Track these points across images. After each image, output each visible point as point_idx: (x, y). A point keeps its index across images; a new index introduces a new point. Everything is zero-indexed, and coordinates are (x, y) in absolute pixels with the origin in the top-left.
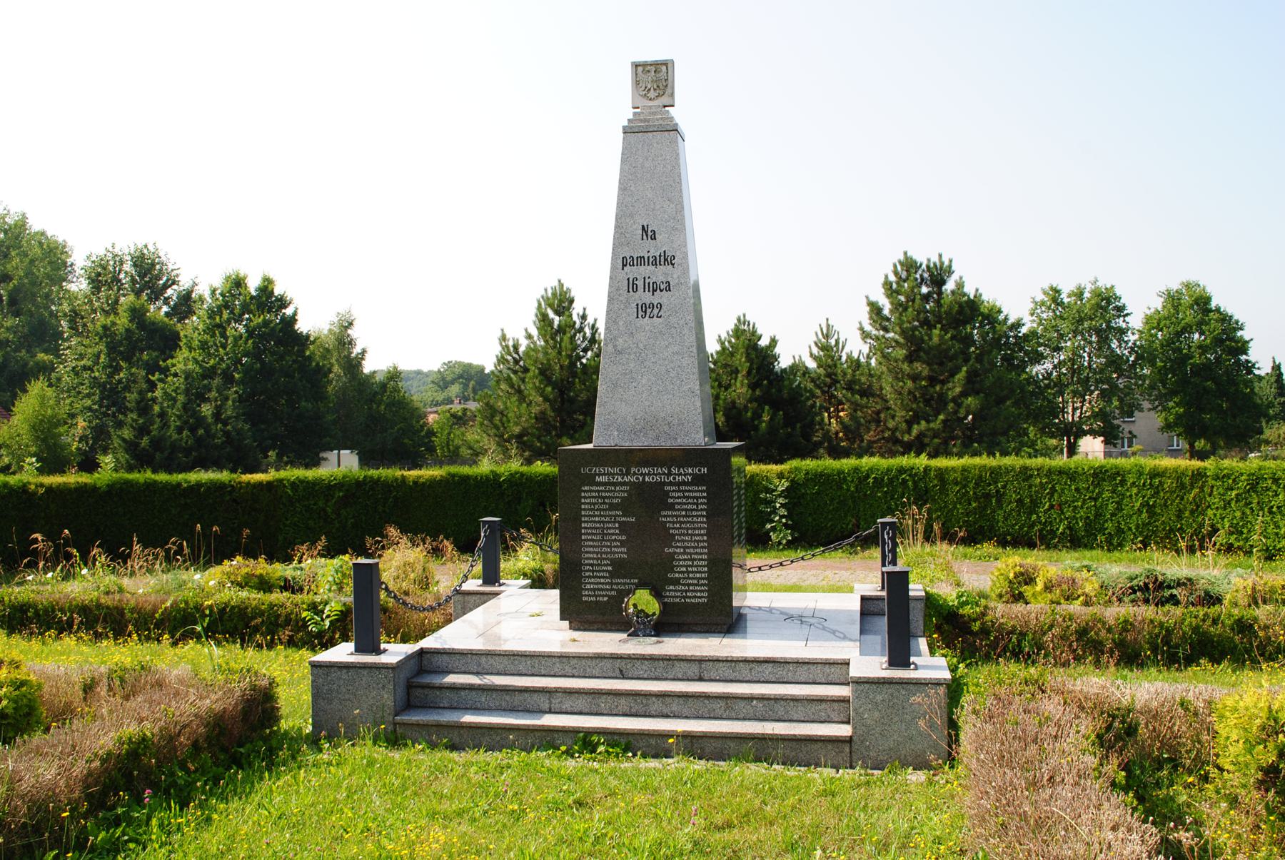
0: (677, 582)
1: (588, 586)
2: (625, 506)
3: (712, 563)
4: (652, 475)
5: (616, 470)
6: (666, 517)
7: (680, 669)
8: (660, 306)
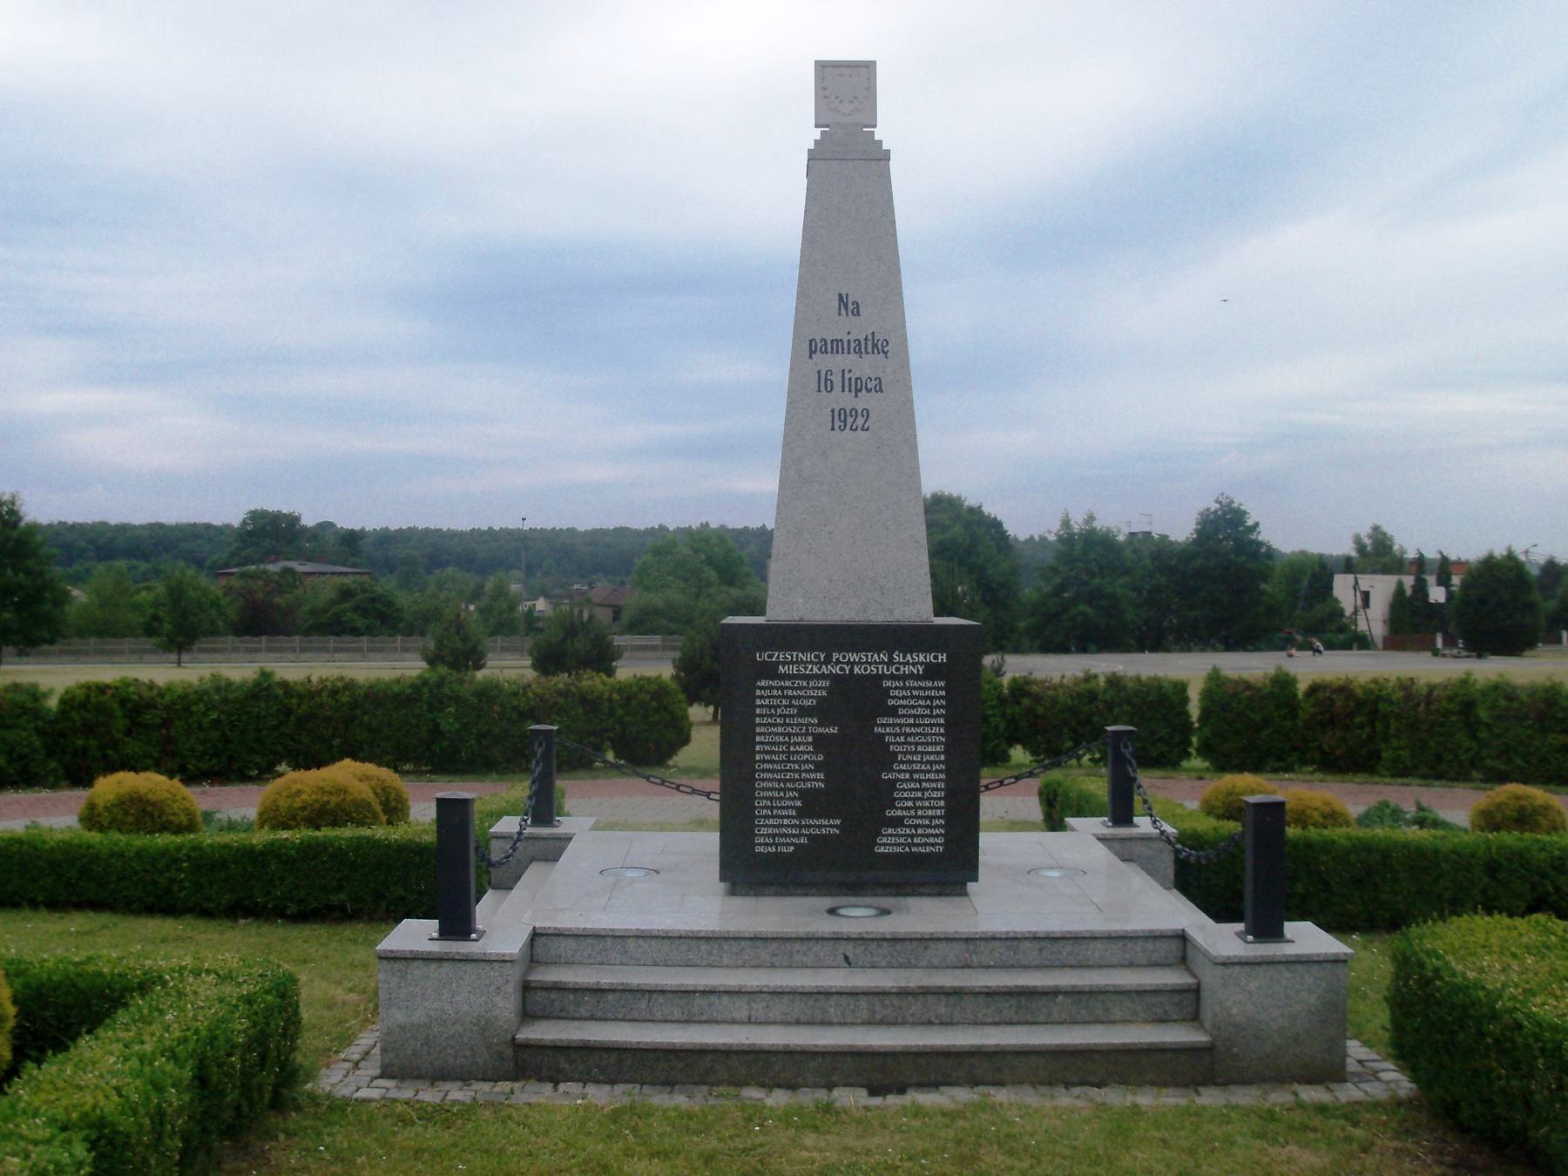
0: (898, 822)
1: (764, 831)
2: (822, 710)
3: (951, 793)
4: (867, 663)
5: (810, 656)
6: (884, 726)
7: (1096, 951)
8: (866, 414)
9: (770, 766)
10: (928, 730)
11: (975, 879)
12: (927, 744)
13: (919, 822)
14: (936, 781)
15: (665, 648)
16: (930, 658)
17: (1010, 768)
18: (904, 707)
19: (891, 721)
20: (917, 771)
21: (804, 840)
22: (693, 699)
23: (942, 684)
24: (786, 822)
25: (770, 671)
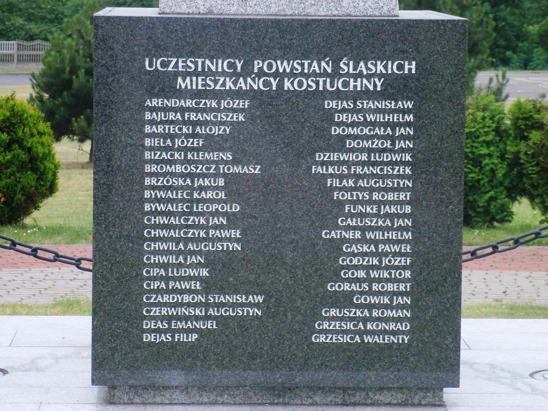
0: (344, 300)
1: (155, 311)
2: (237, 143)
5: (223, 65)
6: (325, 165)
9: (164, 220)
10: (387, 170)
11: (455, 384)
12: (386, 190)
13: (374, 300)
14: (398, 242)
15: (21, 60)
16: (393, 67)
17: (510, 231)
18: (355, 137)
19: (335, 157)
20: (371, 229)
21: (211, 325)
22: (61, 131)
23: (409, 105)
24: (187, 298)
25: (164, 85)
